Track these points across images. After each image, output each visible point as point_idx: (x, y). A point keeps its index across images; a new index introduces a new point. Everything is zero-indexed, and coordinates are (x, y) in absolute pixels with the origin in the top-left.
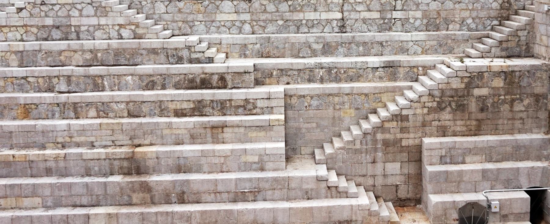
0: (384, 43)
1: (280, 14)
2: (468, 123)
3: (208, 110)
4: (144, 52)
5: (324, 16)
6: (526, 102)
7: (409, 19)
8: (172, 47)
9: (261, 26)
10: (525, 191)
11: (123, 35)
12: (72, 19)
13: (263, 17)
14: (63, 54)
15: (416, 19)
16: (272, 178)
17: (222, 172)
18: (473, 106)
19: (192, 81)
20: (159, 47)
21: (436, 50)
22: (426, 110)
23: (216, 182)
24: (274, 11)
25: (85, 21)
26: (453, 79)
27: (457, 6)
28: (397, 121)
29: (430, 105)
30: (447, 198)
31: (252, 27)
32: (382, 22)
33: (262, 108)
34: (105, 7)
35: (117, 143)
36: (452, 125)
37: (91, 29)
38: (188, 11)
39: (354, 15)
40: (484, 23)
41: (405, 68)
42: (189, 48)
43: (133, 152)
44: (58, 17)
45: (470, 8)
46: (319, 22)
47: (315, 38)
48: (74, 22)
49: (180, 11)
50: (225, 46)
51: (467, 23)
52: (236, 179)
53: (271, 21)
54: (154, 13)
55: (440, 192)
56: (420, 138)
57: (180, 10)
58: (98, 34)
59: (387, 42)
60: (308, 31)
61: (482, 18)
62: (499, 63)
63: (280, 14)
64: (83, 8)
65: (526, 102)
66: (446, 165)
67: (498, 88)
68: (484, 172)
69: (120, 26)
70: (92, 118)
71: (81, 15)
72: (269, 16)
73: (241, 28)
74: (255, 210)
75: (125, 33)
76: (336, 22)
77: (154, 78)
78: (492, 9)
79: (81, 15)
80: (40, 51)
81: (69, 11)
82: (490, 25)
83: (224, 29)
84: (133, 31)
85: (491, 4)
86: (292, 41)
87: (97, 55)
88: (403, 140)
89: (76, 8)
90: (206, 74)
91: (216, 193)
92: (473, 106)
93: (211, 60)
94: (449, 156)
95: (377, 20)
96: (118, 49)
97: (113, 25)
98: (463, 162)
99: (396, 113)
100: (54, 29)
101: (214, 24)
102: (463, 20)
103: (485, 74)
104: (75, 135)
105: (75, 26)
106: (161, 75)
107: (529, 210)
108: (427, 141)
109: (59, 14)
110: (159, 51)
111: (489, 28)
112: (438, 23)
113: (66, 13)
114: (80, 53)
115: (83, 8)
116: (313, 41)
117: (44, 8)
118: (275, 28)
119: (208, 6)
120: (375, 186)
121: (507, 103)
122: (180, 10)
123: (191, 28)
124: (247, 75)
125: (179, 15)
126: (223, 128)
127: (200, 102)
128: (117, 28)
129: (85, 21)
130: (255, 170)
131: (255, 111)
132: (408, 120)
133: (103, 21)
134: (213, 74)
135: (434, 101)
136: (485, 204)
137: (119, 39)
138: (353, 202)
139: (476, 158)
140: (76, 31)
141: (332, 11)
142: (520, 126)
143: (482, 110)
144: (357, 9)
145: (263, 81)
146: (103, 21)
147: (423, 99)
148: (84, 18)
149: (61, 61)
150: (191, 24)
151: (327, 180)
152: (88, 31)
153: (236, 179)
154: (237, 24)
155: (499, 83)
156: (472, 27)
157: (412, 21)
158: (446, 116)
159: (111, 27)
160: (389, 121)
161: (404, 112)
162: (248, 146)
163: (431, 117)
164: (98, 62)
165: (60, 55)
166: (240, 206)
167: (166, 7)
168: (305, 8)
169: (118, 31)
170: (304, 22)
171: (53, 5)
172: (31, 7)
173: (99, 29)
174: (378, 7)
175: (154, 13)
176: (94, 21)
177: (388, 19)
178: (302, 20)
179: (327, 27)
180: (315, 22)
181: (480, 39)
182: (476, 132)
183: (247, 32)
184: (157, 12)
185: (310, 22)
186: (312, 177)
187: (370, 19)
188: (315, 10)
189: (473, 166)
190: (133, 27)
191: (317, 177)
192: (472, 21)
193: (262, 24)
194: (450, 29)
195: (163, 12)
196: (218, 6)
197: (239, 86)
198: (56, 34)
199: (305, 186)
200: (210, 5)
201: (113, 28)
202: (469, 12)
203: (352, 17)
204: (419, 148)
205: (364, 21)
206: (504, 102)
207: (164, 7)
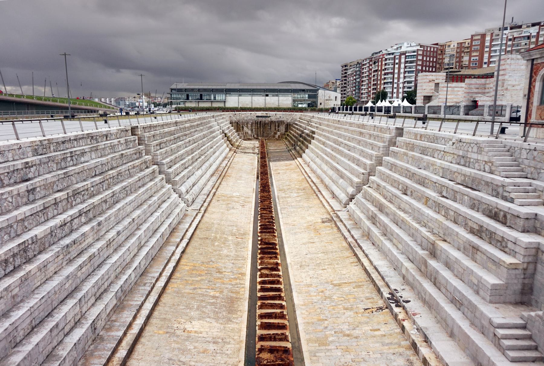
4: (483, 183)
19: (491, 211)
33: (510, 250)
38: (538, 160)
42: (503, 186)
49: (534, 159)
54: (520, 158)
57: (534, 157)
93: (512, 201)
122: (534, 157)
123: (538, 173)
124: (519, 219)
125: (533, 162)
134: (501, 210)
145: (540, 231)
148: (473, 154)
150: (539, 171)
167: (527, 154)
175: (520, 158)
184: (522, 157)
197: (513, 226)
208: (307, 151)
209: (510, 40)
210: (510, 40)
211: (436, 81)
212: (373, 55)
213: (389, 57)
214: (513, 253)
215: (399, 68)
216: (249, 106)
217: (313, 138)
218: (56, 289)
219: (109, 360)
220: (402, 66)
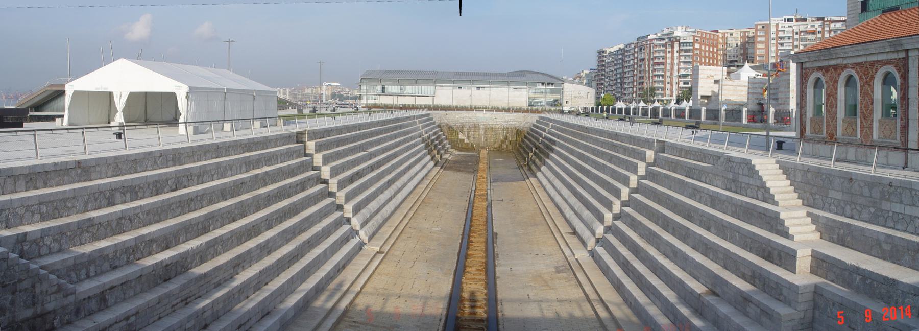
134: (775, 249)
180: (900, 217)
188: (901, 202)
208: (543, 168)
209: (796, 33)
210: (796, 33)
211: (716, 78)
212: (638, 39)
213: (659, 42)
214: (787, 302)
215: (672, 58)
216: (467, 104)
217: (552, 150)
218: (229, 172)
219: (319, 325)
220: (676, 55)
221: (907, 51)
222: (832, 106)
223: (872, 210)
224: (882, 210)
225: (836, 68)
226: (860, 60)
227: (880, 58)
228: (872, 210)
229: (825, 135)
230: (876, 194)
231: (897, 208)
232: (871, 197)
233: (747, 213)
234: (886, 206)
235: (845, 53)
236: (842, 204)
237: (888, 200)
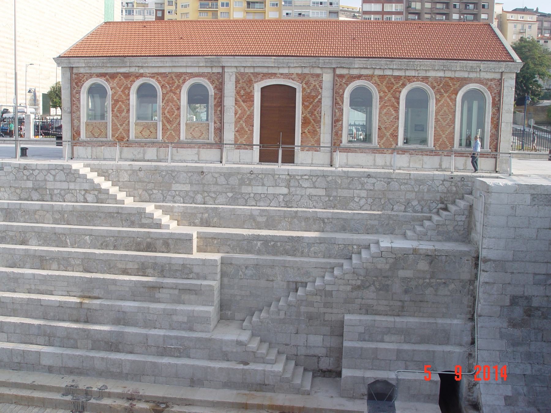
0: (326, 221)
1: (230, 186)
2: (391, 303)
3: (150, 271)
5: (271, 190)
6: (452, 286)
7: (354, 197)
8: (126, 212)
9: (211, 197)
10: (439, 374)
11: (88, 199)
12: (48, 183)
13: (213, 188)
14: (37, 213)
15: (361, 198)
16: (196, 338)
17: (155, 328)
18: (397, 287)
19: (139, 244)
20: (115, 211)
21: (377, 229)
22: (349, 288)
23: (147, 336)
24: (224, 183)
25: (58, 185)
26: (378, 259)
27: (402, 187)
28: (321, 296)
29: (354, 282)
30: (358, 373)
31: (204, 198)
32: (327, 199)
34: (73, 174)
35: (71, 293)
36: (375, 304)
37: (62, 192)
39: (299, 191)
40: (429, 206)
41: (340, 246)
43: (81, 303)
44: (36, 181)
45: (416, 190)
46: (266, 195)
47: (259, 211)
48: (49, 186)
50: (176, 214)
51: (412, 205)
52: (164, 336)
53: (221, 193)
55: (355, 367)
56: (343, 313)
58: (68, 197)
59: (328, 219)
60: (255, 204)
61: (427, 200)
62: (426, 246)
63: (230, 186)
64: (56, 174)
65: (452, 286)
66: (364, 342)
67: (424, 272)
68: (399, 351)
69: (86, 191)
70: (54, 270)
71: (55, 180)
72: (219, 188)
73: (194, 198)
74: (177, 365)
75: (89, 197)
76: (282, 197)
77: (108, 239)
78: (438, 192)
79: (55, 180)
80: (20, 209)
81: (45, 176)
82: (436, 208)
83: (177, 198)
84: (96, 196)
85: (438, 187)
86: (237, 213)
87: (64, 216)
88: (326, 315)
89: (51, 174)
90: (152, 238)
91: (145, 345)
92: (397, 287)
94: (369, 334)
95: (323, 198)
96: (81, 212)
97: (80, 190)
98: (382, 341)
99: (321, 288)
100: (34, 191)
101: (169, 193)
102: (408, 202)
103: (410, 256)
104: (39, 283)
105: (50, 189)
106: (113, 237)
107: (438, 393)
108: (347, 317)
109: (38, 178)
110: (115, 215)
111: (435, 210)
112: (383, 203)
113: (43, 178)
114: (51, 213)
115: (56, 174)
116: (258, 214)
117: (26, 172)
118: (224, 200)
119: (165, 176)
120: (297, 355)
121: (432, 287)
126: (159, 288)
127: (143, 264)
128: (83, 192)
129: (58, 185)
130: (184, 329)
131: (191, 276)
132: (331, 295)
133: (72, 186)
135: (358, 279)
136: (394, 383)
137: (84, 202)
138: (268, 368)
139: (394, 338)
140: (50, 194)
141: (279, 186)
142: (444, 310)
143: (406, 292)
144: (303, 185)
146: (72, 186)
147: (347, 277)
148: (57, 183)
149: (36, 219)
150: (151, 192)
151: (246, 345)
152: (60, 194)
153: (164, 335)
154: (191, 194)
155: (423, 265)
156: (417, 209)
157: (357, 199)
158: (370, 295)
159: (78, 191)
160: (313, 295)
161: (328, 288)
162: (180, 307)
163: (355, 294)
164: (64, 222)
165: (35, 214)
166: (165, 360)
168: (253, 182)
169: (84, 195)
170: (252, 195)
171: (33, 170)
172: (16, 171)
173: (69, 193)
174: (324, 185)
176: (65, 186)
177: (333, 196)
178: (250, 194)
179: (273, 202)
180: (263, 196)
181: (421, 221)
182: (400, 313)
183: (199, 201)
185: (258, 196)
186: (232, 341)
187: (315, 196)
188: (263, 185)
189: (389, 345)
190: (96, 193)
191: (237, 341)
192: (417, 203)
193: (213, 195)
194: (395, 210)
195: (126, 180)
196: (174, 177)
197: (180, 251)
198: (35, 195)
199: (224, 349)
200: (167, 175)
201: (79, 193)
202: (414, 193)
203: (298, 192)
204: (342, 324)
205: (310, 197)
206: (430, 285)
207: (127, 176)
221: (223, 67)
222: (120, 111)
223: (230, 195)
224: (242, 194)
225: (127, 76)
226: (162, 70)
227: (189, 70)
228: (230, 195)
229: (110, 137)
230: (234, 181)
231: (260, 190)
232: (228, 184)
233: (86, 216)
234: (245, 189)
235: (145, 63)
236: (191, 194)
237: (249, 185)
